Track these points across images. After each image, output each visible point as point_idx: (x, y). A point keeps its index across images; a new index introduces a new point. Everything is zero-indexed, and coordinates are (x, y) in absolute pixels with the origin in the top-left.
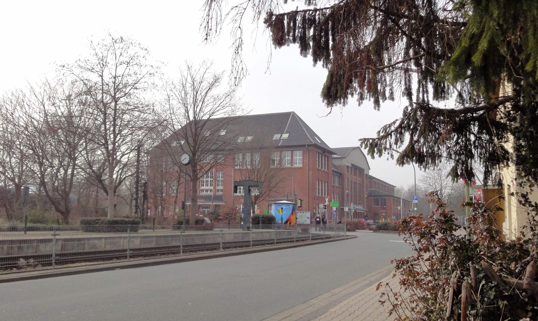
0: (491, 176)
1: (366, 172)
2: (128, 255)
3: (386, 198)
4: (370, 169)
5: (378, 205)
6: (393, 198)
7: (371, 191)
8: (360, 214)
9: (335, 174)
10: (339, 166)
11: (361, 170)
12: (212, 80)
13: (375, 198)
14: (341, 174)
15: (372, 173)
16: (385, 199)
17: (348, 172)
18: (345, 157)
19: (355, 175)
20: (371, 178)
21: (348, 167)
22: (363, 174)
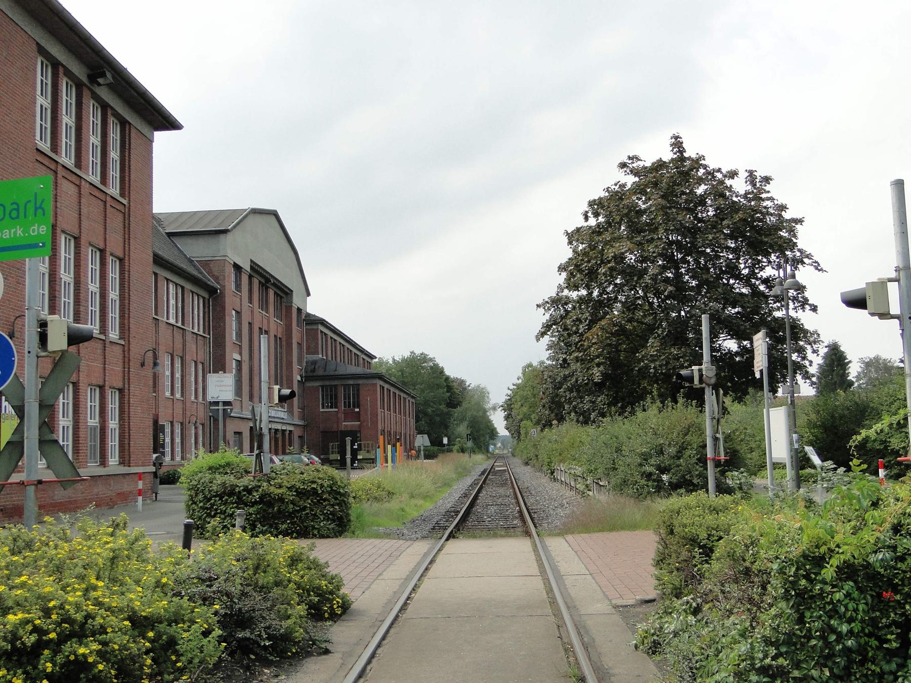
0: (729, 337)
1: (296, 301)
2: (222, 408)
3: (360, 382)
4: (308, 294)
5: (334, 405)
6: (381, 383)
7: (314, 363)
8: (279, 435)
9: (163, 273)
10: (206, 264)
11: (284, 293)
12: (658, 537)
13: (327, 383)
14: (212, 291)
15: (314, 307)
16: (357, 388)
17: (238, 286)
18: (225, 232)
19: (264, 305)
20: (314, 322)
21: (237, 268)
22: (289, 308)
